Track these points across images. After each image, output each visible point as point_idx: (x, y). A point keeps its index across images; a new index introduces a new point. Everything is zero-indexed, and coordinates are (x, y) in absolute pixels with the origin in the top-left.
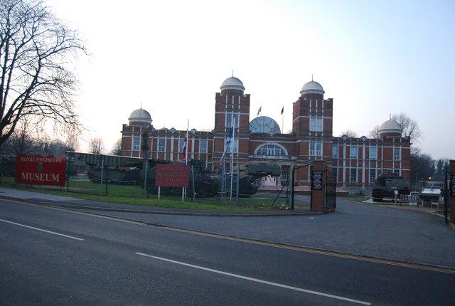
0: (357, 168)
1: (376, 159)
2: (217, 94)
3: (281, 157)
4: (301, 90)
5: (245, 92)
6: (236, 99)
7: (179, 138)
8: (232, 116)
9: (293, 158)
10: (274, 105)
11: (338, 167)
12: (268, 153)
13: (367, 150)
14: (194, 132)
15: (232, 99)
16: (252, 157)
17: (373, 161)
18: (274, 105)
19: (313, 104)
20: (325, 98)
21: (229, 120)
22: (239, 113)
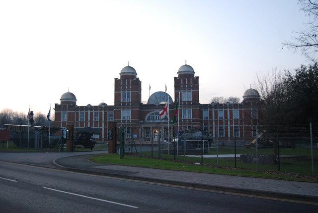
1: (239, 118)
2: (175, 78)
3: (151, 121)
4: (120, 72)
5: (196, 75)
6: (189, 81)
7: (93, 111)
10: (157, 82)
11: (209, 126)
13: (231, 112)
15: (128, 82)
16: (142, 122)
17: (236, 120)
18: (157, 82)
19: (187, 80)
21: (124, 97)
22: (131, 92)
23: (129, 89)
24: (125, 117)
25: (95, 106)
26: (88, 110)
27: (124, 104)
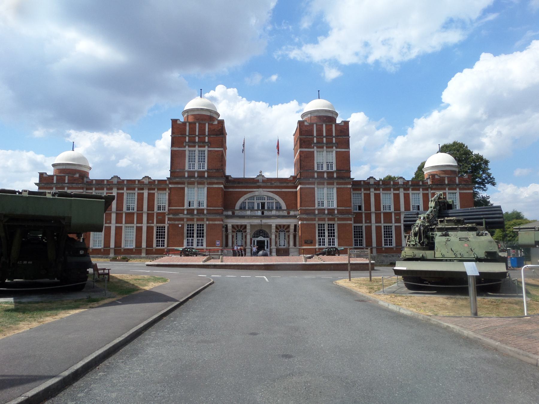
0: (394, 225)
3: (248, 213)
8: (197, 153)
9: (292, 213)
11: (364, 225)
12: (256, 208)
14: (146, 181)
16: (230, 213)
20: (339, 121)
22: (206, 149)
23: (202, 143)
24: (323, 204)
25: (159, 181)
26: (112, 189)
27: (191, 175)
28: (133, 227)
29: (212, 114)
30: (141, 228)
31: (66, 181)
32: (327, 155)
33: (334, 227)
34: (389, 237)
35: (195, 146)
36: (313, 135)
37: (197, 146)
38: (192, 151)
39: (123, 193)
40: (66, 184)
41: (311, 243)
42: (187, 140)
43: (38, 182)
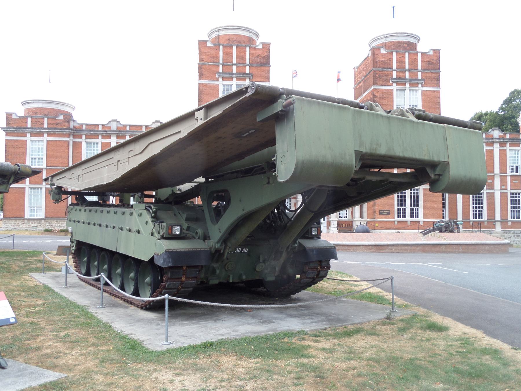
14: (114, 126)
28: (41, 189)
29: (251, 35)
30: (493, 194)
31: (46, 126)
32: (410, 95)
33: (418, 193)
34: (479, 207)
35: (231, 79)
36: (391, 68)
37: (234, 79)
38: (228, 85)
39: (81, 142)
40: (45, 129)
41: (388, 214)
42: (221, 71)
43: (5, 126)
